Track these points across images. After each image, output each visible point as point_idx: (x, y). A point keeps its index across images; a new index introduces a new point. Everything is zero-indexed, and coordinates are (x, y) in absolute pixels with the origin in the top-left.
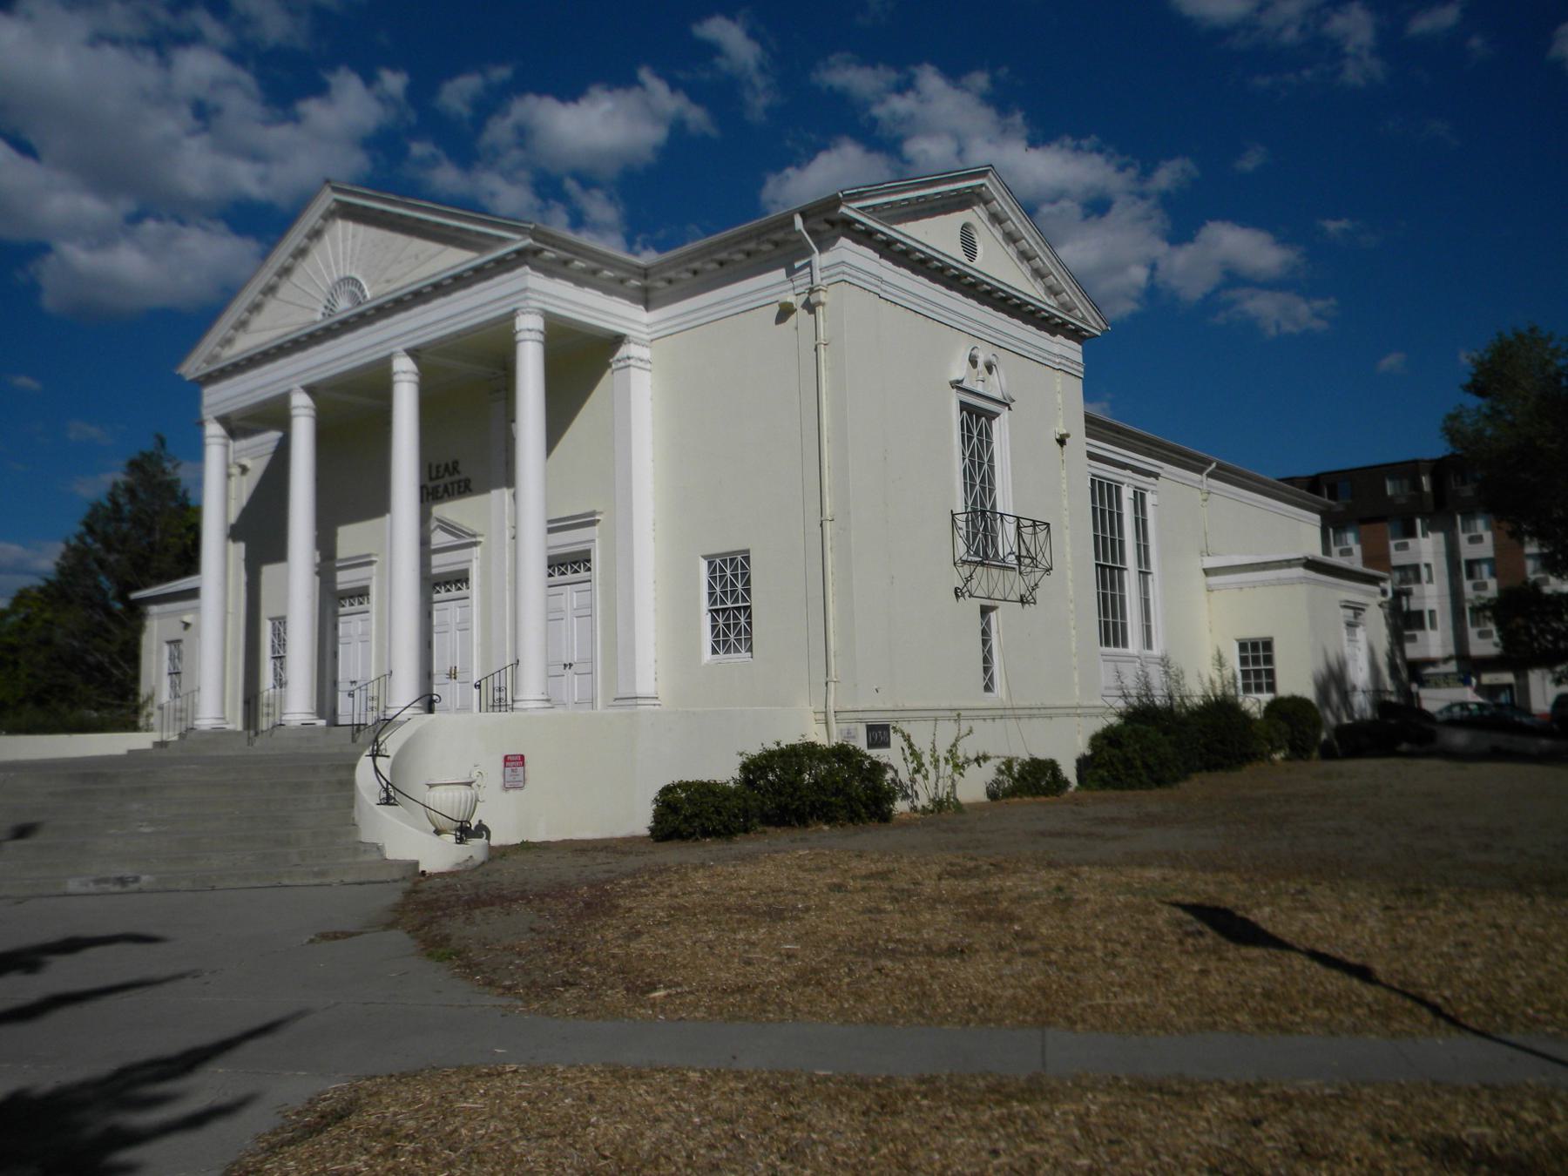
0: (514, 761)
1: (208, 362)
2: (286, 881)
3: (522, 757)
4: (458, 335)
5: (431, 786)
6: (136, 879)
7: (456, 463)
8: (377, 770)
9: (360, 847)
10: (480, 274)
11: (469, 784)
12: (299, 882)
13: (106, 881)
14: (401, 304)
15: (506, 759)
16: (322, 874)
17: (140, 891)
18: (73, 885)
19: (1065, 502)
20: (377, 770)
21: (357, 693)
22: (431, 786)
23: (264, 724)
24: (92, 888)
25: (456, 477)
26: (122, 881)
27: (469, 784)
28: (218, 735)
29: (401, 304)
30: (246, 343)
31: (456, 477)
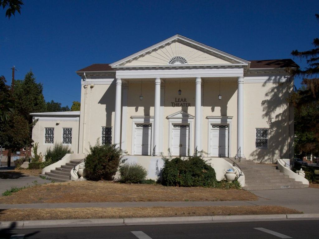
14: (195, 67)
17: (289, 188)
24: (284, 188)
30: (134, 64)
31: (186, 102)
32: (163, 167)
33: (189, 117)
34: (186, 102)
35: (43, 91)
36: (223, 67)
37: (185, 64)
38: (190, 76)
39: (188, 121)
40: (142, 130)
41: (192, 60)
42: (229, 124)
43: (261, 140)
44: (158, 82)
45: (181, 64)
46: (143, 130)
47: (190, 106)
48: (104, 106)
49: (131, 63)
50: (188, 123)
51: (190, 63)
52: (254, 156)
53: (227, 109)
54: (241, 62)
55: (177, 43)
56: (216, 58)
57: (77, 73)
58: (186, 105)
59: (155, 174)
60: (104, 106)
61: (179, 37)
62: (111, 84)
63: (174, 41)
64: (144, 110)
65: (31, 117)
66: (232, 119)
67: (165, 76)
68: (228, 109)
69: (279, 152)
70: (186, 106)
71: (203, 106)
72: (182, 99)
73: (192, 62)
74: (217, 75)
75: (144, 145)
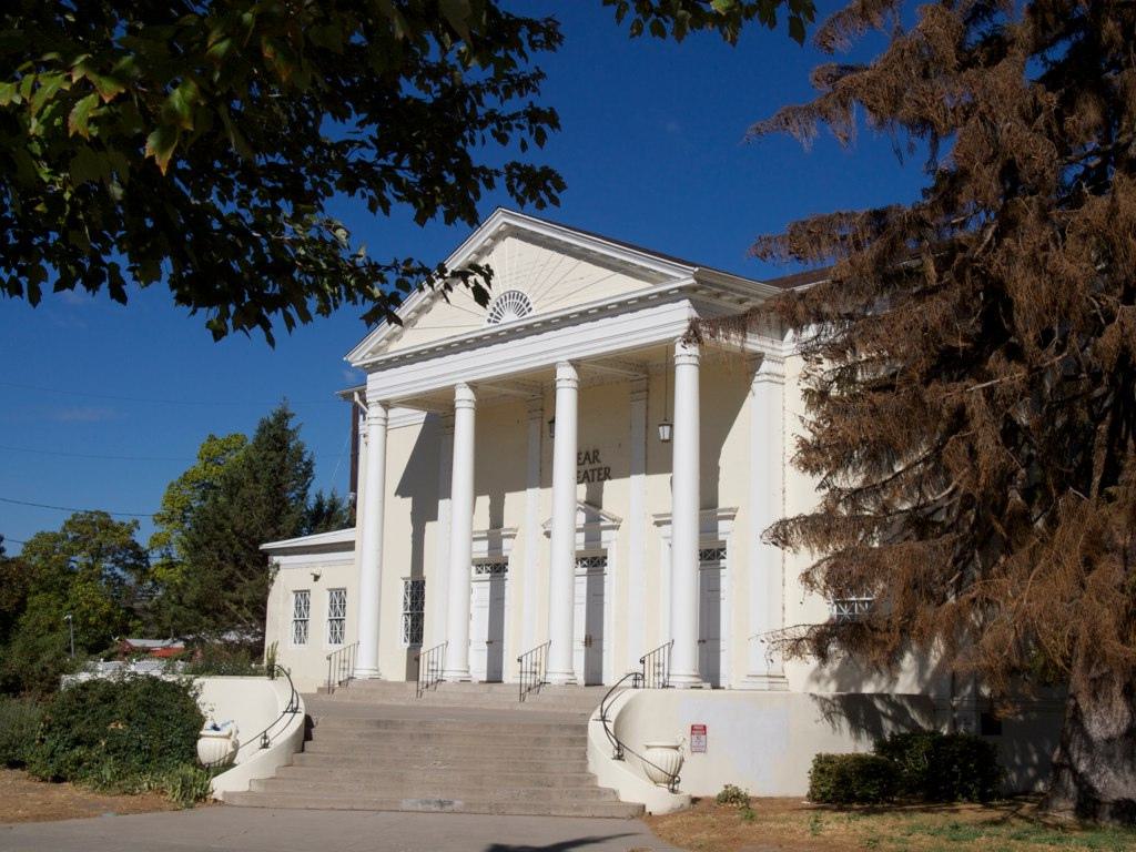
0: (699, 730)
1: (374, 352)
2: (553, 813)
3: (705, 727)
4: (619, 351)
5: (648, 747)
6: (450, 803)
7: (596, 452)
8: (606, 729)
9: (600, 792)
10: (644, 302)
11: (676, 748)
12: (562, 814)
13: (429, 803)
14: (566, 321)
15: (693, 728)
16: (578, 809)
17: (453, 812)
18: (406, 805)
19: (1001, 309)
20: (606, 729)
21: (524, 659)
22: (648, 747)
23: (424, 676)
24: (420, 807)
25: (597, 465)
26: (442, 804)
27: (676, 748)
28: (376, 682)
29: (566, 321)
30: (410, 340)
31: (597, 465)
32: (872, 743)
33: (602, 524)
34: (599, 461)
35: (314, 469)
36: (624, 307)
37: (528, 315)
38: (541, 360)
39: (501, 547)
40: (488, 584)
41: (547, 296)
42: (725, 541)
43: (852, 610)
44: (464, 397)
45: (517, 318)
46: (589, 583)
47: (610, 478)
48: (408, 501)
49: (402, 339)
50: (504, 554)
51: (540, 310)
52: (823, 682)
53: (718, 479)
54: (674, 277)
55: (509, 239)
56: (609, 272)
57: (343, 395)
58: (599, 474)
59: (810, 760)
60: (408, 501)
61: (506, 217)
62: (423, 420)
63: (498, 237)
64: (491, 507)
65: (266, 555)
66: (669, 522)
67: (477, 374)
68: (722, 475)
69: (914, 663)
70: (599, 480)
71: (647, 474)
72: (587, 454)
73: (546, 302)
74: (629, 338)
75: (704, 641)
